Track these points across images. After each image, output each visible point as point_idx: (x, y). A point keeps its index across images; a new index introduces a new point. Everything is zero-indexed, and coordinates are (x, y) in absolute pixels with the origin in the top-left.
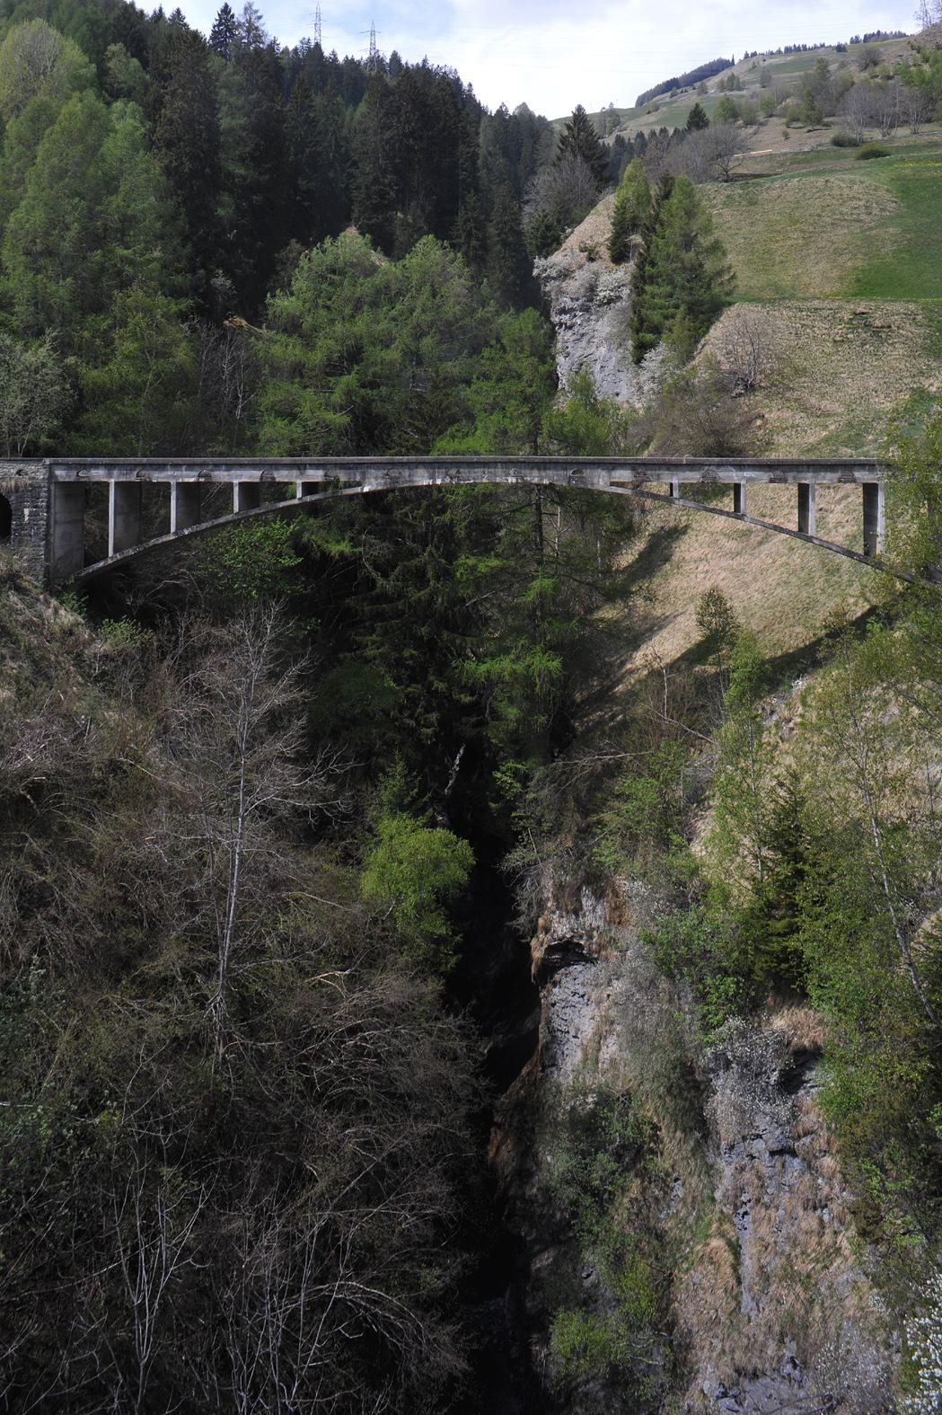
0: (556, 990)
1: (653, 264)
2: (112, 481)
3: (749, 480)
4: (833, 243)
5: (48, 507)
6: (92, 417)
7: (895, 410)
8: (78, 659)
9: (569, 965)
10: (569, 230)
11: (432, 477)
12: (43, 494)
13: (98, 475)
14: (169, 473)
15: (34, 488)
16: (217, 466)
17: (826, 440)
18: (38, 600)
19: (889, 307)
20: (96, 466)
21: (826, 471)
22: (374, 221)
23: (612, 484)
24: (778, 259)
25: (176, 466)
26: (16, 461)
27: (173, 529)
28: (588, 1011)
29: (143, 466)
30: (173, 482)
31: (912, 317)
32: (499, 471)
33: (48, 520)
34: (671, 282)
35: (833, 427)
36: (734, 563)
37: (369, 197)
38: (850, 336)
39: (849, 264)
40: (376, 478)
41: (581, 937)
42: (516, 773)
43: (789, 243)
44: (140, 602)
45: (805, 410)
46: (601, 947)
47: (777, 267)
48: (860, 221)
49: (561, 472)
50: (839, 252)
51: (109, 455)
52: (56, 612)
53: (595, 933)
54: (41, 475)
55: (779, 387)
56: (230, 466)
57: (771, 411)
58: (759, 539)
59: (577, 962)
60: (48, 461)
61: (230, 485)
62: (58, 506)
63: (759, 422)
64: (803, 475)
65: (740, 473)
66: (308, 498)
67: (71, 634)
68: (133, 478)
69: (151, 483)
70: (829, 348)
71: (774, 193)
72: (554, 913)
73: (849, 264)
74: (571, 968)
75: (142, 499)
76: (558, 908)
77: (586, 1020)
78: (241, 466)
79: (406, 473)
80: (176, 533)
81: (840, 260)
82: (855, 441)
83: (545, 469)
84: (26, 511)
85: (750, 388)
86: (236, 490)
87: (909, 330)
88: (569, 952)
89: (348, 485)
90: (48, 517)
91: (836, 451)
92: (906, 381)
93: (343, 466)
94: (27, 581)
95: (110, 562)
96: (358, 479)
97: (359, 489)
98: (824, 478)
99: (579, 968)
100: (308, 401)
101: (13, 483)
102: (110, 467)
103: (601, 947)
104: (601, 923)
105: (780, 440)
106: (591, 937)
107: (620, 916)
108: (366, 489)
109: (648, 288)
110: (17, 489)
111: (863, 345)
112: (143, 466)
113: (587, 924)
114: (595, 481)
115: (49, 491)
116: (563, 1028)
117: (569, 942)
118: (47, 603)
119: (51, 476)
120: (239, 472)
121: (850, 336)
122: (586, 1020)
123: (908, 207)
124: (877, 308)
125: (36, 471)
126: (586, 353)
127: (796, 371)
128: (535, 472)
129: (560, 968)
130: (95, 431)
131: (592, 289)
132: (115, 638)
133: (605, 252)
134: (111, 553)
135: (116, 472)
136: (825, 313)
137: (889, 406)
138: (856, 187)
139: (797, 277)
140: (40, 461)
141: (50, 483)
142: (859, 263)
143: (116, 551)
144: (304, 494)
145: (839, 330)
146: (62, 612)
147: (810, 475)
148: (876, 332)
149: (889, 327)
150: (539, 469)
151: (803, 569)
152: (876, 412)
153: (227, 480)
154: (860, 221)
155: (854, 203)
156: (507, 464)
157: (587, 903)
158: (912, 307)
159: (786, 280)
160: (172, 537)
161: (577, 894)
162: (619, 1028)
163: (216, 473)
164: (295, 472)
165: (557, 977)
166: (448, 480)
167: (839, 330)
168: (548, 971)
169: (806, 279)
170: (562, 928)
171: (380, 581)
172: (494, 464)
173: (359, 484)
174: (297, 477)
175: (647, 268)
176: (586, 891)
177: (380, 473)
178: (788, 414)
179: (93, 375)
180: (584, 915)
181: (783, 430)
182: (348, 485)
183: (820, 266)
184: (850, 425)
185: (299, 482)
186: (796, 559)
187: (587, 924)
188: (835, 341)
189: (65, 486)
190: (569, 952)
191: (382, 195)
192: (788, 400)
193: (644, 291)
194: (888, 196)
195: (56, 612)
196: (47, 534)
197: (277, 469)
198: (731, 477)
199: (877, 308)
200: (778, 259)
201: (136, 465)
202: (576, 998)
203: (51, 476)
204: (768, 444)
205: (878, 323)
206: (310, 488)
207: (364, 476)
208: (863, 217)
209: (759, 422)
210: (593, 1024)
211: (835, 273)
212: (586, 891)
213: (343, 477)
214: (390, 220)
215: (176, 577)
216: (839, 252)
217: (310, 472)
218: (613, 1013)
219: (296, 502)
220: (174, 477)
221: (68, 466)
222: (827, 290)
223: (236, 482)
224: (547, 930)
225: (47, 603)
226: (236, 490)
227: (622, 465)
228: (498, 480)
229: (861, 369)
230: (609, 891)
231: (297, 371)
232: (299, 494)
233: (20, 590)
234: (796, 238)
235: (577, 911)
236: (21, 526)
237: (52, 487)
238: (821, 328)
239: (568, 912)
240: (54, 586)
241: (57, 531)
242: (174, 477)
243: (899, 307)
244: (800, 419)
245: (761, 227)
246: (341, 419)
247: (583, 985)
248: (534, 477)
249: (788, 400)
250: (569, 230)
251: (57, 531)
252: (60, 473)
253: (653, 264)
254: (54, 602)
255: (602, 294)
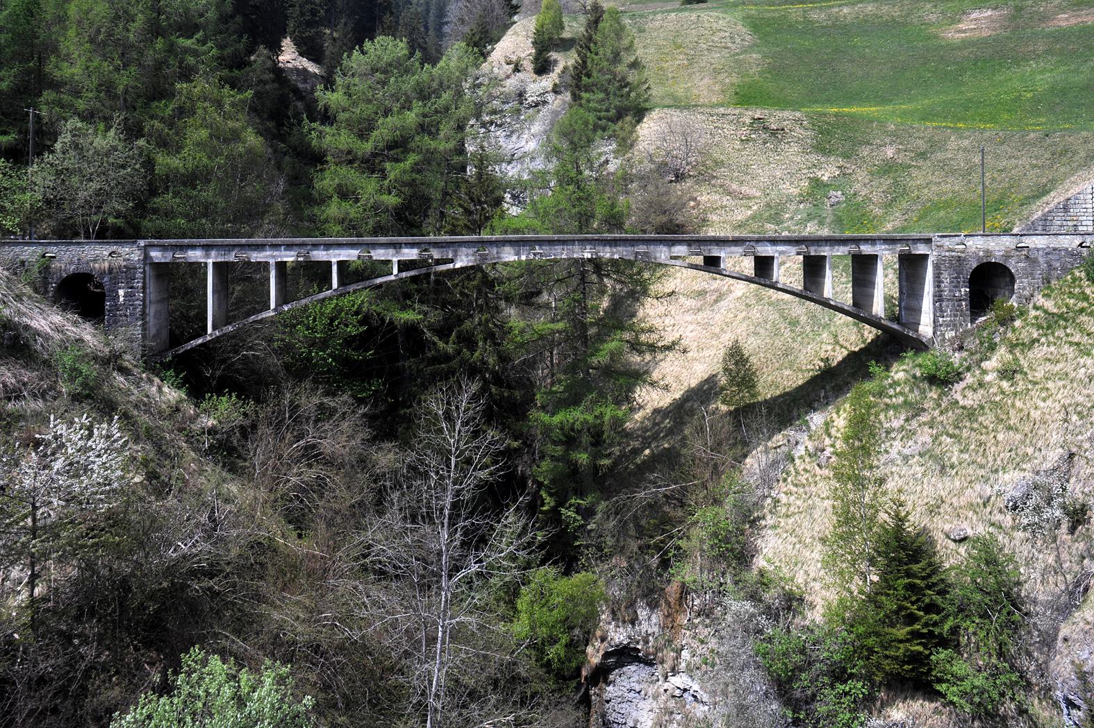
0: (610, 688)
1: (589, 76)
2: (210, 261)
3: (781, 253)
4: (712, 64)
5: (144, 288)
6: (166, 200)
7: (801, 195)
8: (189, 438)
9: (624, 666)
10: (489, 47)
11: (518, 254)
12: (138, 275)
13: (196, 255)
14: (268, 253)
15: (129, 270)
16: (316, 246)
17: (753, 217)
18: (142, 379)
19: (780, 114)
20: (193, 247)
21: (839, 245)
22: (307, 34)
23: (672, 258)
24: (670, 75)
25: (275, 246)
26: (108, 243)
27: (273, 306)
28: (646, 705)
29: (242, 246)
30: (272, 261)
31: (798, 121)
32: (576, 248)
33: (144, 300)
34: (606, 91)
35: (755, 208)
36: (700, 316)
37: (302, 14)
38: (753, 136)
39: (727, 81)
40: (467, 255)
41: (638, 643)
42: (578, 510)
43: (678, 62)
44: (218, 373)
45: (729, 194)
46: (658, 650)
47: (671, 81)
48: (728, 48)
49: (630, 249)
50: (717, 72)
51: (176, 236)
52: (160, 388)
53: (651, 638)
54: (136, 256)
55: (705, 176)
56: (328, 246)
57: (702, 195)
58: (714, 297)
59: (630, 663)
60: (142, 243)
61: (329, 264)
62: (152, 287)
63: (692, 203)
64: (822, 248)
65: (774, 248)
66: (404, 275)
67: (178, 410)
68: (231, 257)
69: (249, 263)
70: (738, 145)
71: (657, 24)
72: (610, 623)
73: (727, 81)
74: (625, 669)
75: (240, 283)
76: (613, 619)
77: (644, 713)
78: (340, 245)
79: (495, 250)
80: (275, 310)
81: (720, 77)
82: (776, 218)
83: (616, 246)
84: (121, 292)
85: (679, 177)
86: (335, 268)
87: (799, 132)
88: (624, 655)
89: (438, 262)
90: (144, 297)
91: (762, 226)
92: (804, 171)
93: (436, 245)
94: (128, 360)
95: (209, 338)
96: (450, 256)
97: (451, 266)
98: (838, 251)
99: (633, 668)
100: (369, 187)
101: (106, 265)
102: (207, 248)
103: (658, 650)
104: (656, 629)
105: (713, 217)
106: (647, 642)
107: (673, 621)
108: (458, 265)
109: (585, 95)
110: (111, 270)
111: (765, 143)
112: (242, 246)
113: (643, 631)
114: (658, 255)
115: (144, 272)
116: (620, 720)
117: (626, 647)
118: (151, 381)
119: (147, 256)
120: (337, 252)
121: (753, 136)
122: (644, 713)
123: (760, 39)
124: (771, 115)
125: (130, 253)
126: (517, 146)
127: (716, 162)
128: (608, 249)
129: (614, 670)
130: (169, 214)
131: (521, 95)
132: (220, 413)
133: (528, 65)
134: (210, 330)
135: (213, 253)
136: (731, 118)
137: (796, 191)
138: (721, 22)
139: (688, 89)
140: (135, 243)
141: (145, 264)
142: (735, 80)
143: (214, 328)
144: (400, 271)
145: (744, 131)
146: (166, 389)
147: (827, 248)
148: (774, 133)
149: (783, 130)
150: (610, 246)
151: (766, 322)
152: (787, 196)
153: (325, 259)
154: (728, 48)
155: (722, 34)
156: (583, 242)
157: (642, 613)
158: (798, 114)
159: (680, 91)
160: (272, 314)
161: (632, 605)
162: (679, 717)
163: (315, 253)
164: (391, 251)
165: (611, 677)
166: (532, 257)
167: (744, 131)
168: (601, 674)
169: (696, 91)
170: (619, 636)
171: (441, 345)
172: (573, 241)
173: (452, 261)
174: (393, 255)
175: (584, 78)
176: (641, 603)
177: (471, 251)
178: (717, 197)
179: (166, 162)
180: (640, 624)
181: (715, 210)
182: (438, 262)
183: (706, 81)
184: (768, 205)
185: (395, 260)
186: (755, 314)
187: (643, 631)
188: (742, 140)
189: (159, 268)
190: (624, 655)
191: (314, 13)
192: (714, 186)
193: (580, 98)
194: (744, 30)
195: (160, 388)
196: (144, 314)
197: (374, 249)
198: (767, 251)
199: (771, 115)
200: (670, 75)
201: (234, 246)
202: (632, 694)
203: (147, 256)
204: (704, 220)
205: (774, 127)
206: (404, 266)
207: (456, 255)
208: (730, 45)
209: (692, 203)
210: (652, 715)
211: (717, 88)
212: (641, 603)
213: (436, 254)
214: (320, 35)
215: (251, 348)
216: (717, 72)
217: (406, 251)
218: (672, 704)
219: (392, 278)
220: (273, 257)
221: (164, 248)
222: (714, 100)
223: (334, 260)
224: (603, 639)
225: (151, 381)
226: (335, 268)
227: (680, 242)
228: (575, 256)
229: (766, 162)
230: (662, 602)
231: (350, 158)
232: (395, 271)
233: (124, 371)
234: (681, 59)
235: (634, 621)
236: (116, 307)
237: (147, 268)
238: (729, 130)
239: (624, 622)
240: (155, 363)
241: (151, 310)
242: (273, 257)
243: (786, 114)
244: (726, 200)
245: (652, 50)
246: (392, 200)
247: (638, 682)
248: (607, 253)
249: (714, 186)
250: (489, 47)
251: (151, 310)
252: (156, 255)
253: (589, 76)
254: (157, 380)
255: (530, 99)
